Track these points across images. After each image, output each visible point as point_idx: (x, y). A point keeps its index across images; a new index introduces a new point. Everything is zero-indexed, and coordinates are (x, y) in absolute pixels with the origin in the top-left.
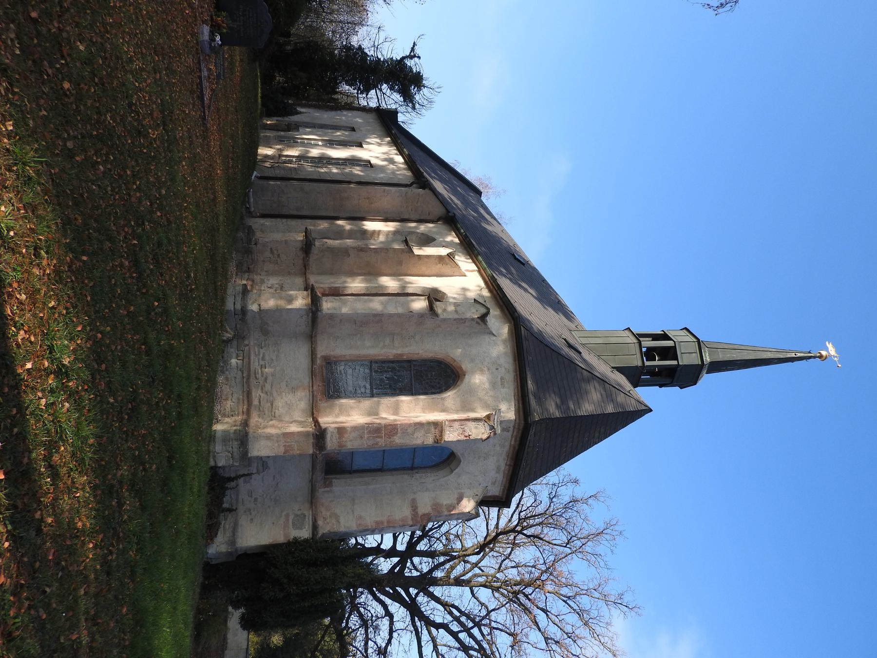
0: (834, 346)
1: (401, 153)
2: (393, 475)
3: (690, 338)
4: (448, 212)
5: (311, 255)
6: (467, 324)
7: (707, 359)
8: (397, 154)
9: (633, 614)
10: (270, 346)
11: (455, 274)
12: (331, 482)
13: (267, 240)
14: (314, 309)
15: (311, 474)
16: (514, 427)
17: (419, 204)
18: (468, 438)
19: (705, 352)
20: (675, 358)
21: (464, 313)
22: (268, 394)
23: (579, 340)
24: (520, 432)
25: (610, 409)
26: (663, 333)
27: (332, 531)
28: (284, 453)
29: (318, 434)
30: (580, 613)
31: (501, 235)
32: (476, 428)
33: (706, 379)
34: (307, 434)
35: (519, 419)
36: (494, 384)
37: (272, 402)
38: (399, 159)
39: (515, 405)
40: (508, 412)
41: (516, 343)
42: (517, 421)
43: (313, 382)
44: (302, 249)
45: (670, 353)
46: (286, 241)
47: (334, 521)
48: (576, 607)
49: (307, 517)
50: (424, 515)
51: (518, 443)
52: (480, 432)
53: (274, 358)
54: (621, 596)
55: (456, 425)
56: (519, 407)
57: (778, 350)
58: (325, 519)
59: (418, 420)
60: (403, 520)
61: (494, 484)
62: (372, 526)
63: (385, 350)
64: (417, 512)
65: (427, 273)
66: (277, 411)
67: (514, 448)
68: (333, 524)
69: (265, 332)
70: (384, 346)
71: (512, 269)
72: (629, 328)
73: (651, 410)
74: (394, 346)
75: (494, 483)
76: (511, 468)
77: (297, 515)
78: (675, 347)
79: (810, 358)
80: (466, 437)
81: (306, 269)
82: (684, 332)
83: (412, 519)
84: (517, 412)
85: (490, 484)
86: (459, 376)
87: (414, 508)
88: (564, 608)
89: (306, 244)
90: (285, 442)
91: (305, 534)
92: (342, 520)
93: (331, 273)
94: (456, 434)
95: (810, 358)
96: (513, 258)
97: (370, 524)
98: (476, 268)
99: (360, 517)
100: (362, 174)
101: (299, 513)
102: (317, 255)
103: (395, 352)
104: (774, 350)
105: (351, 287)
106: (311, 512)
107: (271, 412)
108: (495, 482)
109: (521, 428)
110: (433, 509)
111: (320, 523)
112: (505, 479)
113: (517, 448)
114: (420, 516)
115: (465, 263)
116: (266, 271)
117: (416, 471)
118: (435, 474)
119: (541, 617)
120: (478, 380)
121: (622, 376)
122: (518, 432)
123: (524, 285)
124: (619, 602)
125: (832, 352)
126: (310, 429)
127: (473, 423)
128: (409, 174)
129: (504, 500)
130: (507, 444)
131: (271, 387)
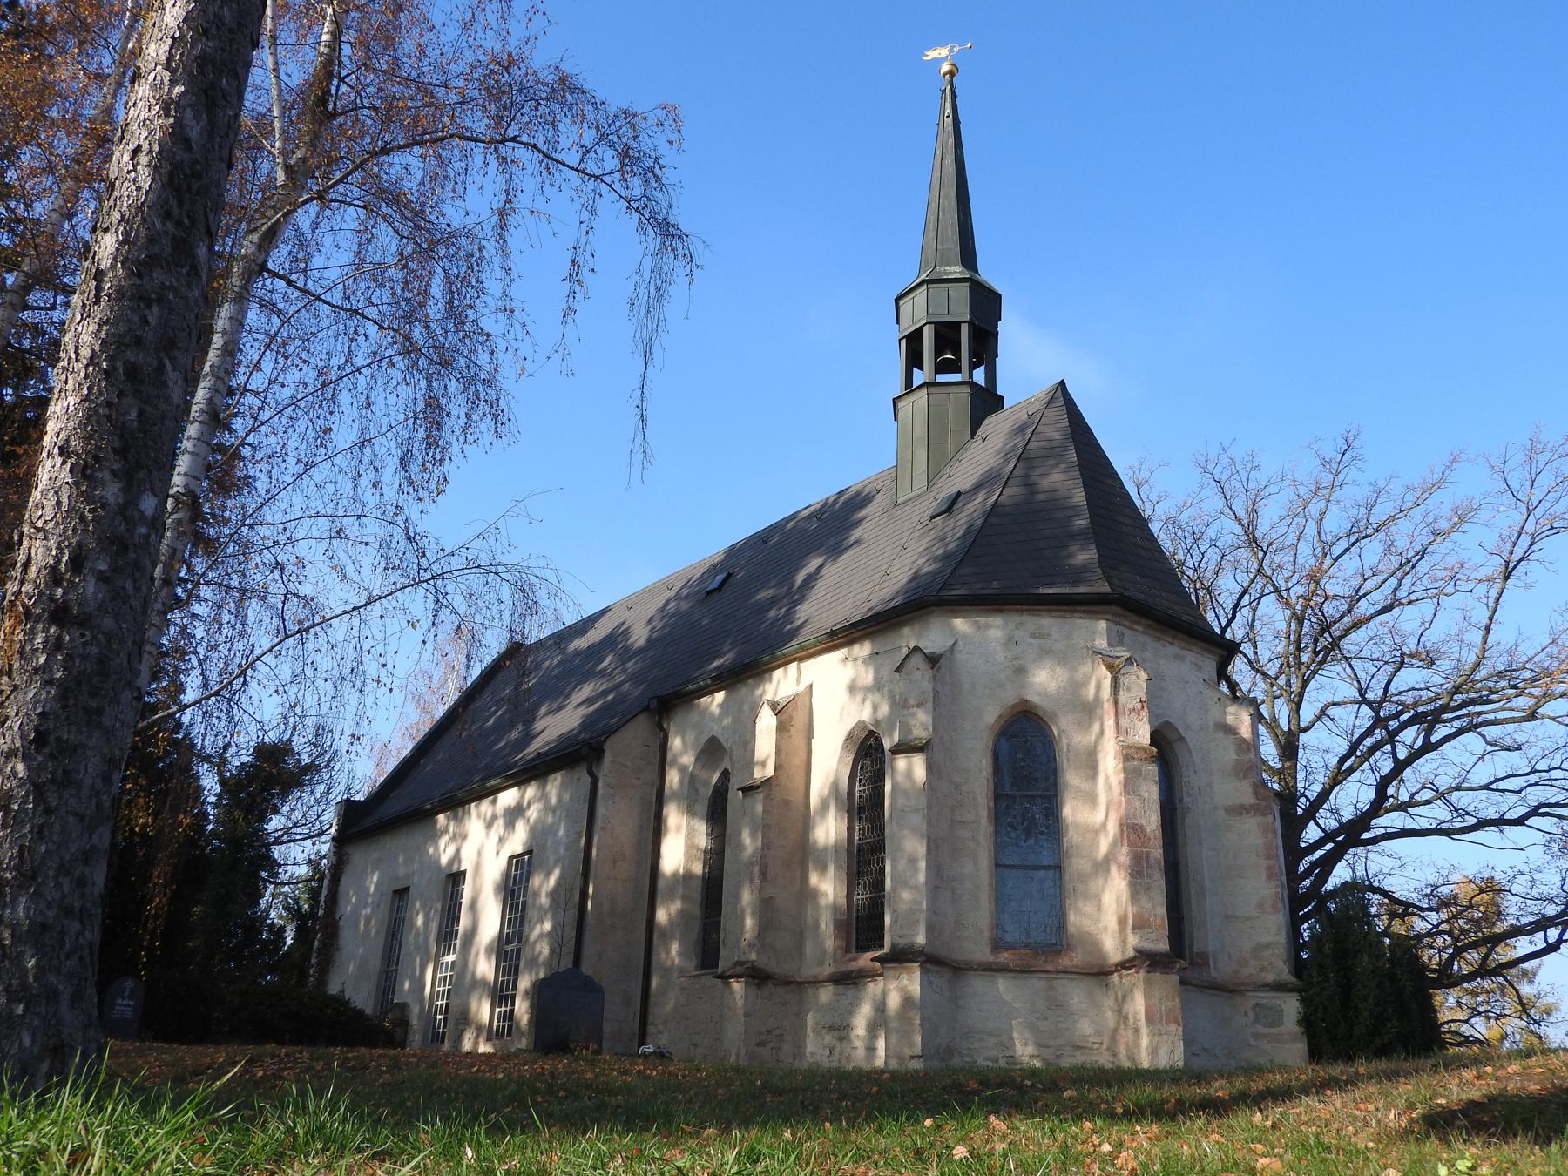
0: (932, 47)
1: (495, 791)
3: (921, 296)
7: (957, 270)
8: (494, 802)
9: (1355, 444)
10: (972, 1046)
11: (808, 705)
13: (743, 1052)
15: (1190, 988)
16: (1117, 624)
17: (629, 764)
18: (1145, 705)
21: (923, 693)
22: (1059, 1053)
23: (919, 492)
24: (1127, 614)
25: (1072, 456)
27: (1285, 957)
28: (1179, 1025)
29: (1147, 963)
30: (1358, 535)
33: (988, 273)
34: (1148, 983)
36: (1042, 650)
37: (1073, 1046)
38: (508, 797)
39: (1081, 618)
40: (1099, 631)
41: (970, 605)
42: (1109, 617)
43: (1040, 971)
44: (758, 986)
45: (946, 335)
46: (746, 1015)
47: (1267, 953)
48: (1343, 544)
49: (1260, 1001)
50: (1256, 794)
51: (1143, 620)
52: (1137, 682)
53: (993, 1040)
54: (1325, 463)
55: (1124, 722)
56: (1084, 612)
58: (1262, 969)
59: (1117, 788)
60: (1265, 832)
61: (1200, 667)
62: (1277, 886)
64: (1251, 806)
65: (803, 756)
66: (1091, 1039)
67: (1148, 626)
69: (950, 1051)
72: (894, 399)
73: (1062, 382)
74: (973, 822)
75: (1199, 668)
76: (1180, 635)
77: (1257, 1020)
78: (936, 324)
79: (953, 93)
80: (1143, 707)
81: (791, 982)
82: (906, 305)
83: (1264, 815)
84: (1096, 615)
85: (1200, 675)
86: (1026, 711)
87: (1241, 810)
88: (1350, 564)
89: (753, 977)
90: (1161, 1021)
91: (1291, 1007)
92: (1266, 939)
93: (799, 936)
94: (1139, 725)
95: (953, 93)
96: (715, 595)
97: (1273, 890)
98: (794, 665)
99: (1260, 906)
100: (557, 873)
101: (1251, 1015)
102: (769, 958)
103: (984, 821)
106: (1250, 994)
107: (1091, 1049)
108: (1196, 664)
110: (1245, 777)
112: (1194, 649)
113: (1149, 622)
114: (1257, 802)
115: (783, 683)
116: (794, 1059)
117: (1177, 802)
118: (1184, 769)
119: (1364, 608)
120: (1045, 680)
121: (986, 422)
122: (1126, 617)
123: (800, 577)
124: (1335, 466)
127: (1121, 693)
128: (555, 786)
129: (1225, 653)
130: (1142, 638)
131: (1048, 1047)
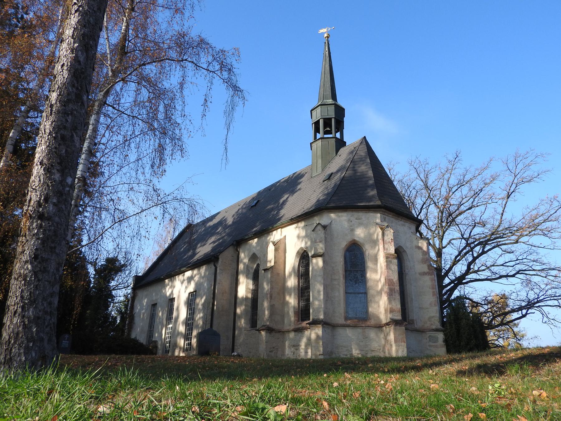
2: (406, 285)
3: (319, 109)
4: (233, 244)
5: (274, 328)
6: (327, 237)
7: (330, 101)
8: (184, 275)
9: (459, 155)
12: (411, 320)
13: (265, 354)
14: (322, 323)
16: (384, 214)
19: (326, 102)
20: (330, 119)
24: (387, 211)
25: (368, 161)
26: (313, 125)
30: (461, 185)
31: (234, 212)
32: (387, 235)
33: (341, 102)
34: (395, 329)
35: (380, 211)
38: (188, 274)
40: (377, 217)
42: (381, 212)
44: (270, 333)
46: (266, 342)
47: (433, 319)
50: (429, 268)
52: (390, 234)
54: (450, 162)
55: (386, 246)
56: (373, 211)
57: (324, 60)
58: (432, 324)
63: (341, 285)
65: (283, 258)
68: (435, 320)
69: (332, 353)
70: (338, 284)
71: (269, 207)
75: (410, 228)
77: (430, 341)
79: (328, 43)
82: (314, 113)
83: (431, 275)
84: (376, 212)
87: (424, 274)
88: (458, 194)
91: (441, 336)
94: (391, 247)
95: (328, 43)
96: (254, 207)
98: (280, 230)
99: (431, 304)
101: (428, 339)
104: (324, 63)
105: (294, 304)
109: (384, 210)
110: (425, 263)
111: (434, 327)
113: (394, 214)
115: (276, 235)
120: (360, 233)
121: (340, 150)
123: (281, 201)
125: (325, 30)
126: (392, 327)
